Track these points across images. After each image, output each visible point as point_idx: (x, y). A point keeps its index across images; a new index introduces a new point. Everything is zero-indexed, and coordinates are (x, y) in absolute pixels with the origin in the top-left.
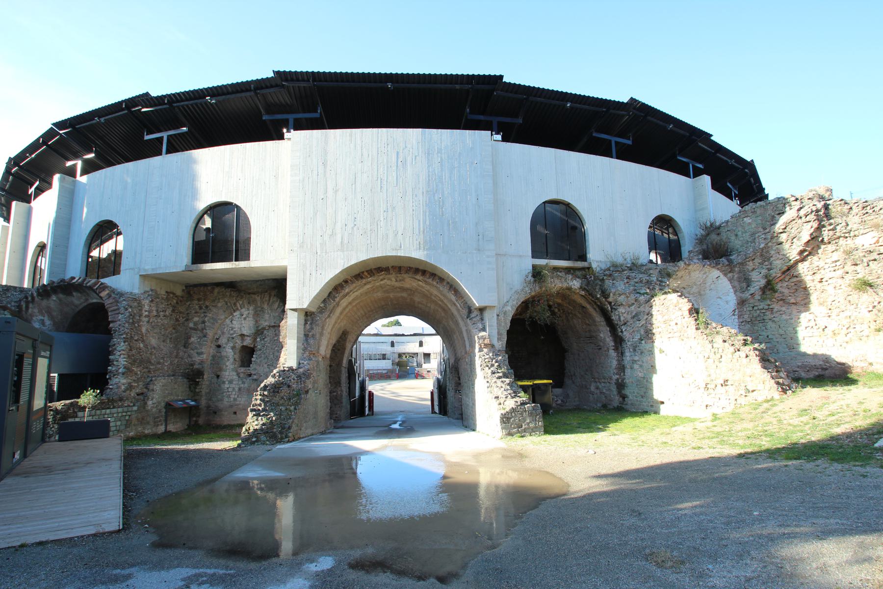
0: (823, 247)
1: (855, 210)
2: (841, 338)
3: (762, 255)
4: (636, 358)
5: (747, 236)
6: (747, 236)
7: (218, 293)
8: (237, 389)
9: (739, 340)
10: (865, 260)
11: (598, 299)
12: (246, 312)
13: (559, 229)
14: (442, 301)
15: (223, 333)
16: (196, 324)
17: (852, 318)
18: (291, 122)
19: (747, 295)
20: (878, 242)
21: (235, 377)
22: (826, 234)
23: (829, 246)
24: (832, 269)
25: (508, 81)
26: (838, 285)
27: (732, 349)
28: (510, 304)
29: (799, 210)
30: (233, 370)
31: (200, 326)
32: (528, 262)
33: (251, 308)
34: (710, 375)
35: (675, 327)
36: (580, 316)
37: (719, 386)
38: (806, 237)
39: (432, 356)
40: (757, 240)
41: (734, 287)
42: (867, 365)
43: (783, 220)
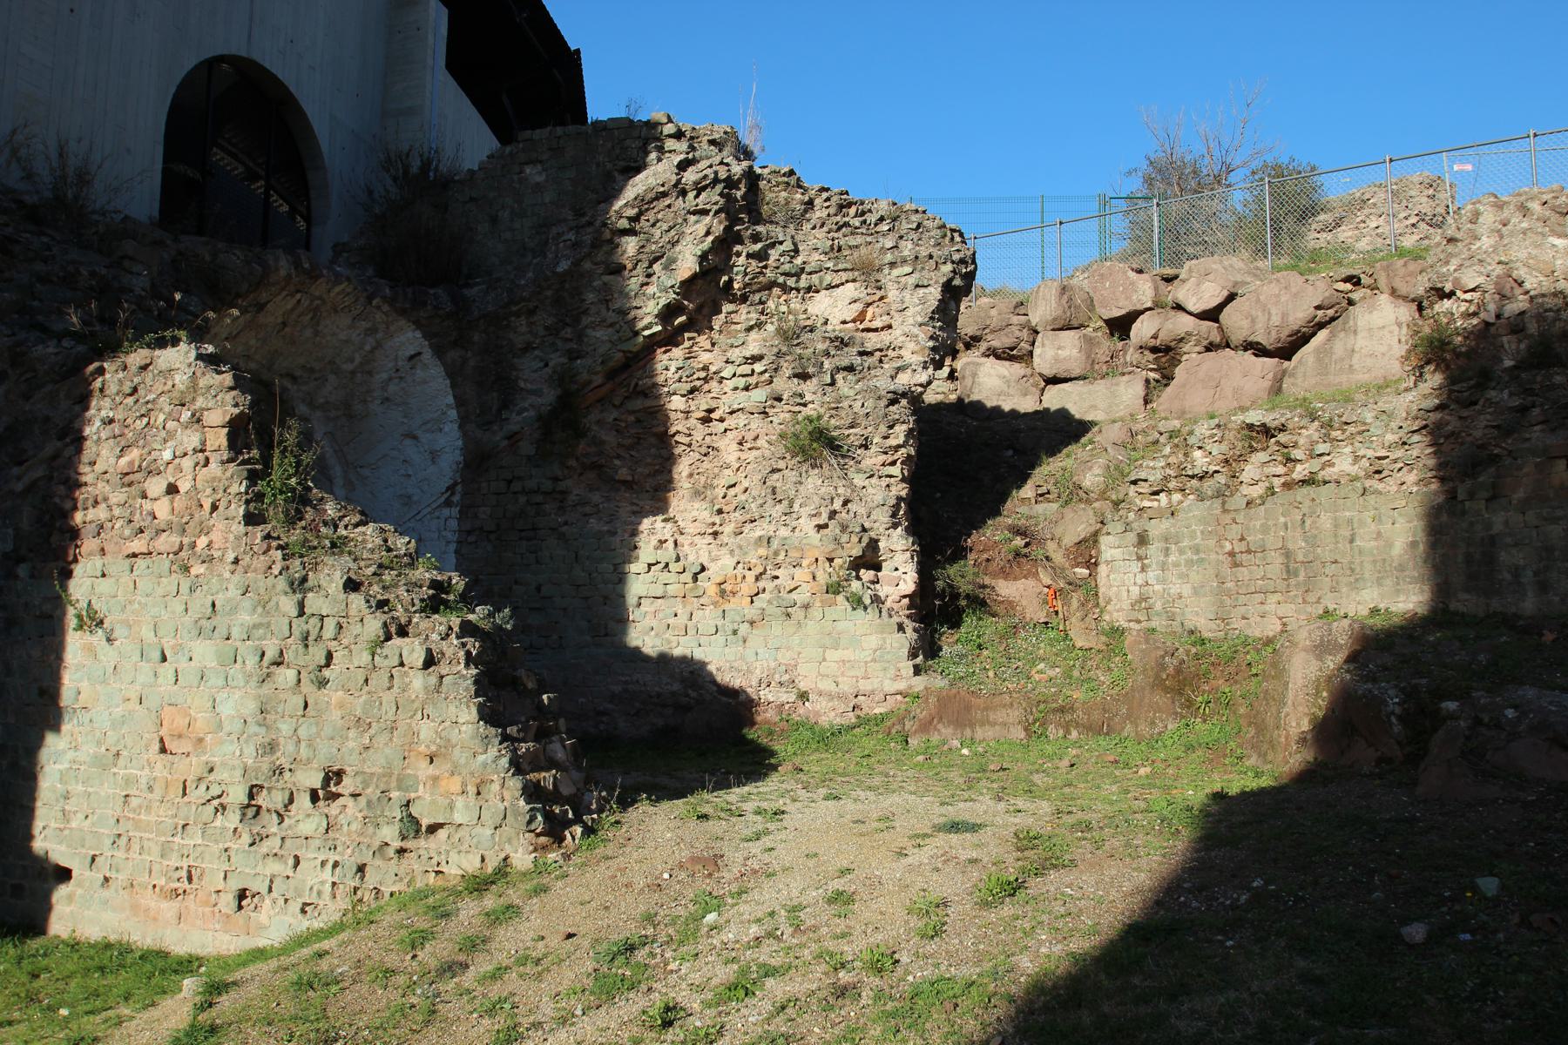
0: (727, 307)
1: (819, 214)
2: (739, 606)
9: (413, 586)
10: (828, 364)
17: (775, 544)
20: (861, 317)
22: (741, 264)
23: (744, 308)
24: (741, 382)
26: (749, 436)
27: (374, 625)
29: (683, 166)
34: (272, 747)
35: (162, 509)
37: (304, 801)
38: (687, 264)
41: (460, 402)
42: (792, 697)
43: (638, 186)
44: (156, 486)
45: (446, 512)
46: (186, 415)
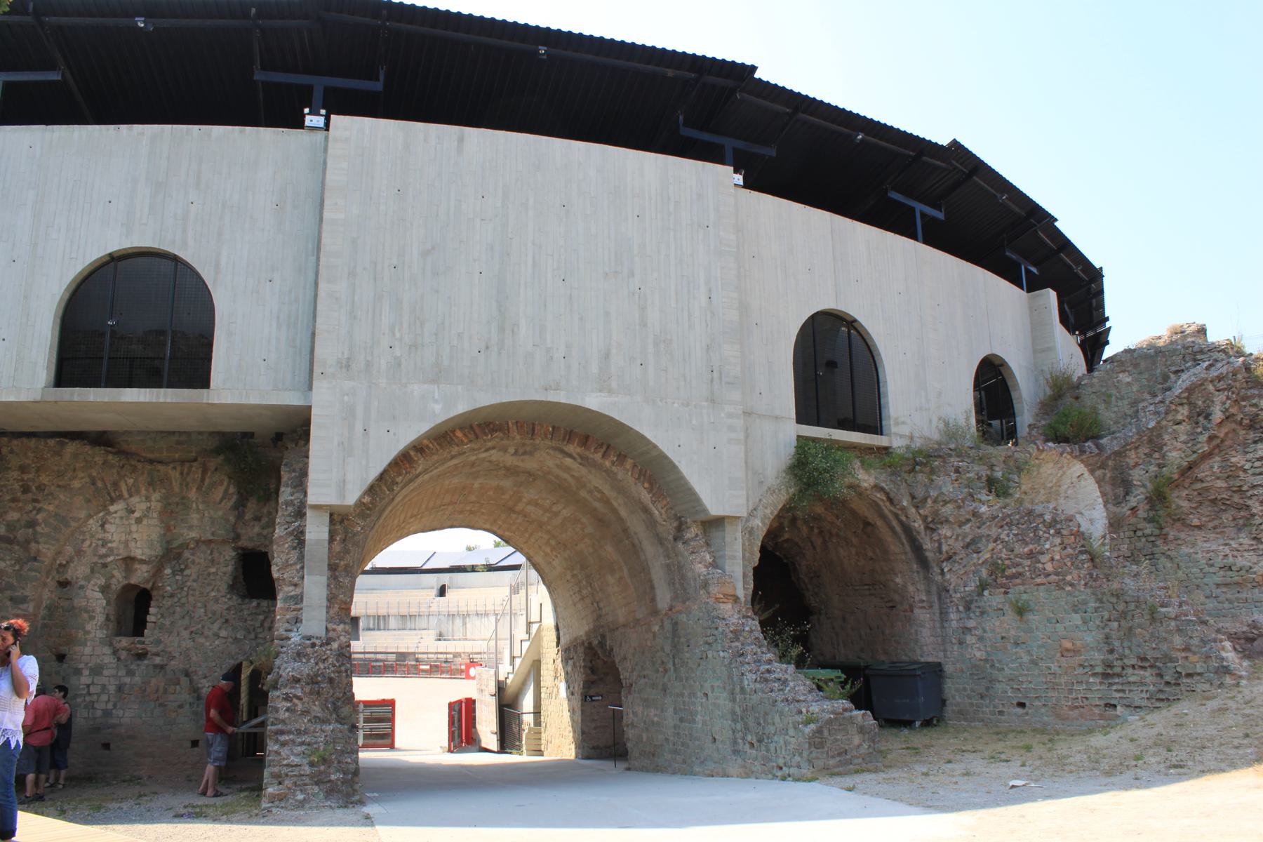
3: (1150, 441)
4: (971, 624)
5: (1124, 405)
6: (1124, 405)
7: (75, 456)
8: (112, 689)
11: (903, 509)
12: (144, 506)
13: (835, 368)
14: (606, 501)
15: (80, 552)
18: (318, 95)
19: (1125, 509)
21: (109, 659)
28: (760, 513)
30: (102, 642)
31: (21, 534)
33: (156, 496)
36: (855, 541)
41: (1104, 494)
46: (1052, 531)
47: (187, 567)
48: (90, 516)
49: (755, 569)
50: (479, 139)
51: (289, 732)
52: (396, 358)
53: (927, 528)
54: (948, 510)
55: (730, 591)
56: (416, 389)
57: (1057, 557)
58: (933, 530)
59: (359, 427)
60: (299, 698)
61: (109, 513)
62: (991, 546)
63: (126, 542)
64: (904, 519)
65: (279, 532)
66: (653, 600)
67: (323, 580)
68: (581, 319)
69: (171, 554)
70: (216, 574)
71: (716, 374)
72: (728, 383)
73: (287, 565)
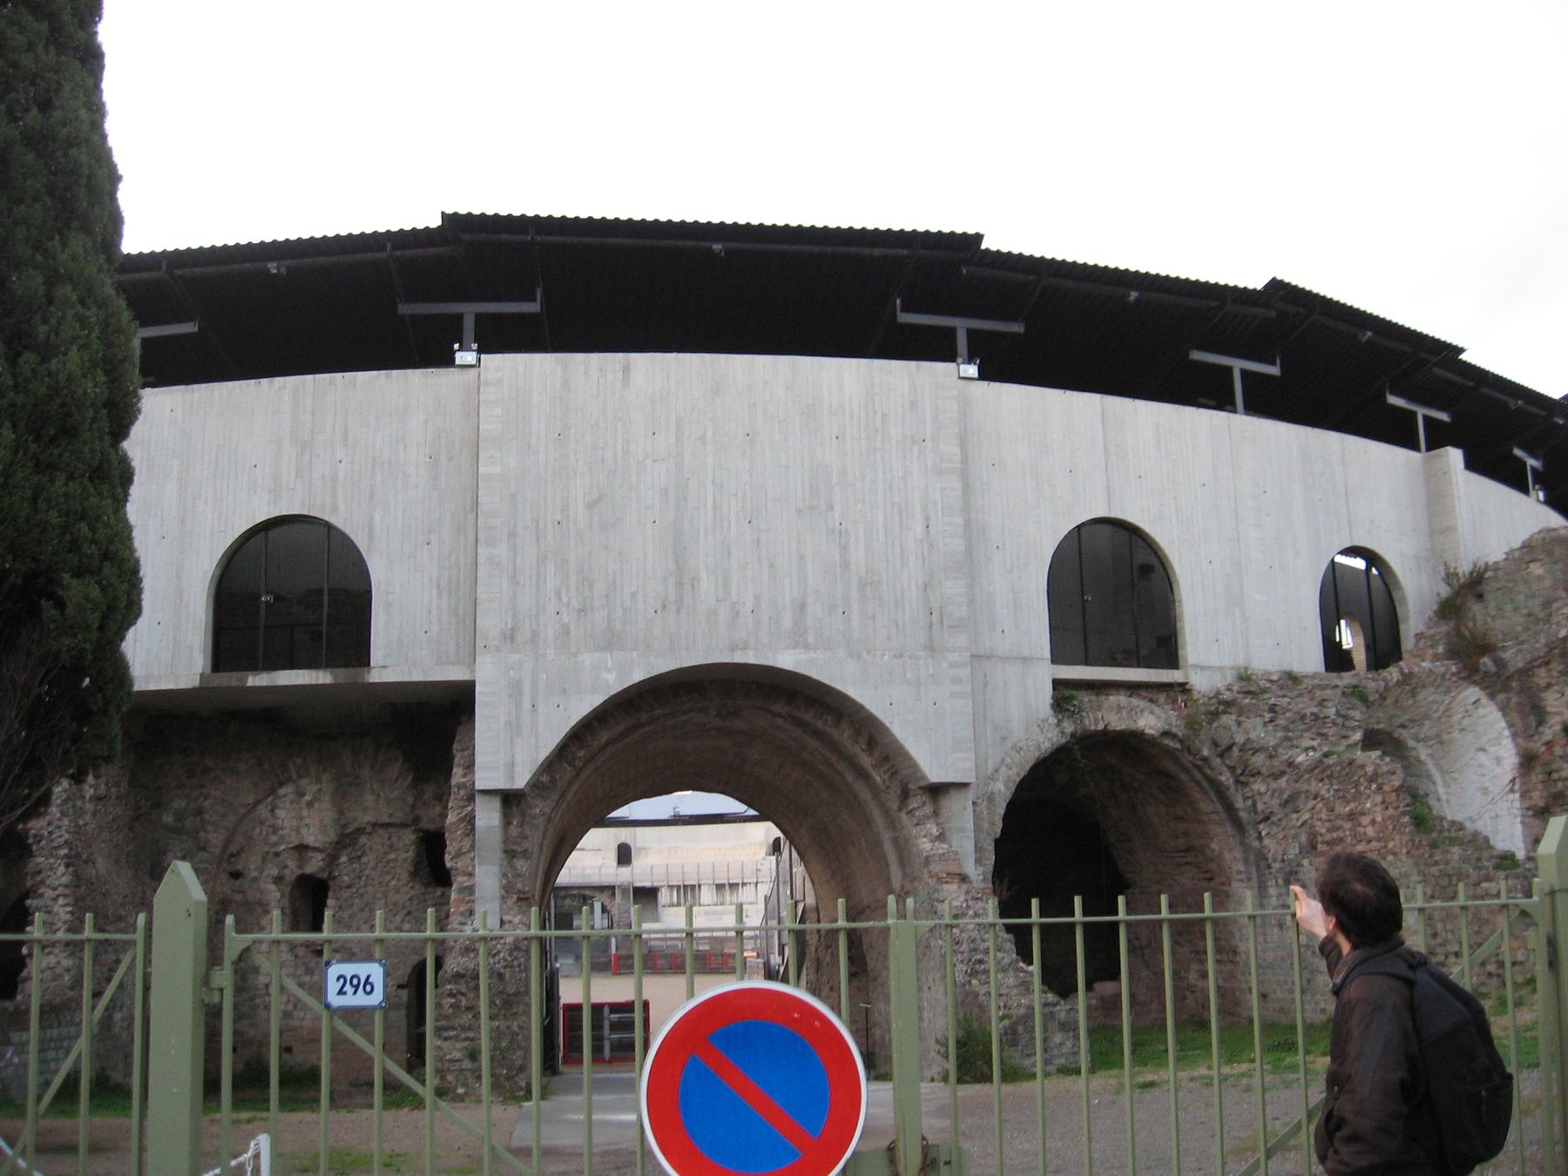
12: (314, 788)
13: (1113, 589)
16: (179, 816)
18: (469, 325)
25: (994, 248)
32: (1045, 673)
39: (664, 897)
40: (1555, 619)
41: (1511, 725)
44: (1365, 820)
45: (1511, 796)
46: (1374, 786)
47: (364, 854)
48: (258, 802)
49: (997, 842)
50: (644, 364)
51: (453, 1028)
52: (564, 625)
53: (1237, 782)
54: (1259, 760)
55: (956, 870)
56: (587, 659)
57: (1379, 819)
58: (1244, 784)
59: (526, 704)
60: (464, 994)
61: (279, 798)
62: (1311, 804)
63: (298, 830)
64: (1208, 771)
65: (452, 818)
66: (889, 879)
67: (495, 869)
68: (771, 566)
69: (346, 840)
70: (396, 860)
71: (935, 617)
72: (950, 627)
73: (459, 854)
